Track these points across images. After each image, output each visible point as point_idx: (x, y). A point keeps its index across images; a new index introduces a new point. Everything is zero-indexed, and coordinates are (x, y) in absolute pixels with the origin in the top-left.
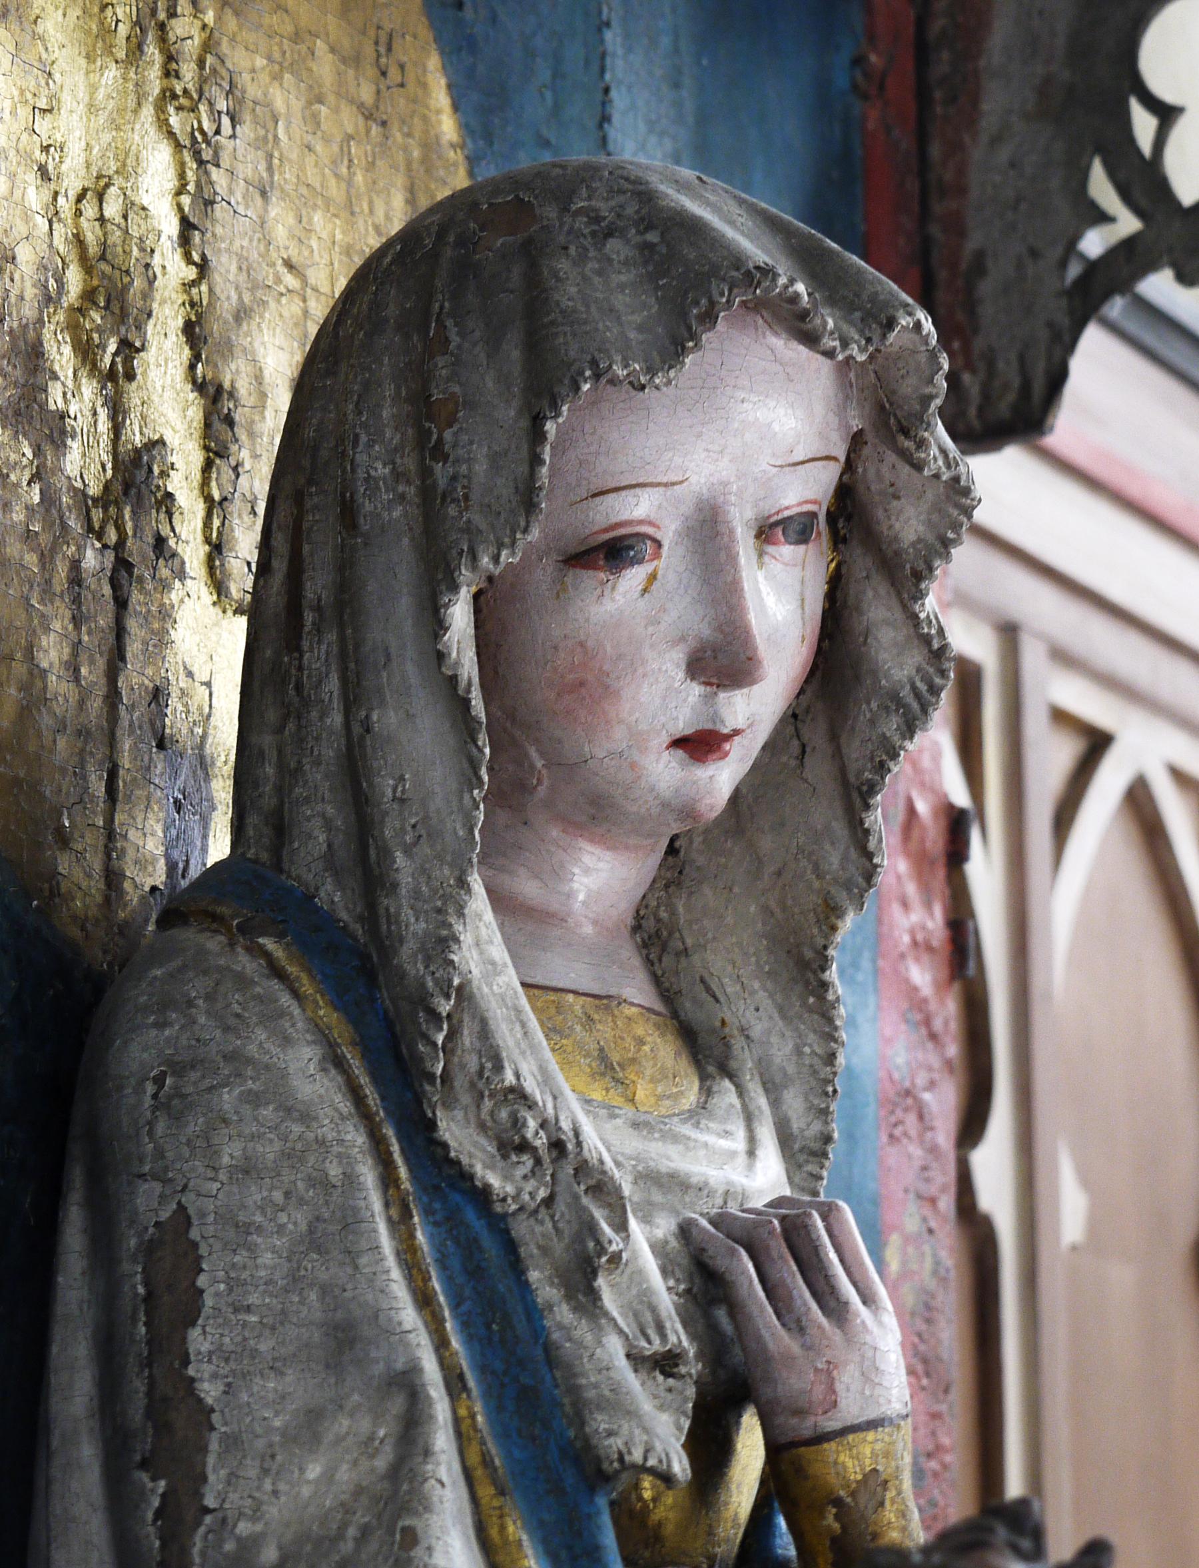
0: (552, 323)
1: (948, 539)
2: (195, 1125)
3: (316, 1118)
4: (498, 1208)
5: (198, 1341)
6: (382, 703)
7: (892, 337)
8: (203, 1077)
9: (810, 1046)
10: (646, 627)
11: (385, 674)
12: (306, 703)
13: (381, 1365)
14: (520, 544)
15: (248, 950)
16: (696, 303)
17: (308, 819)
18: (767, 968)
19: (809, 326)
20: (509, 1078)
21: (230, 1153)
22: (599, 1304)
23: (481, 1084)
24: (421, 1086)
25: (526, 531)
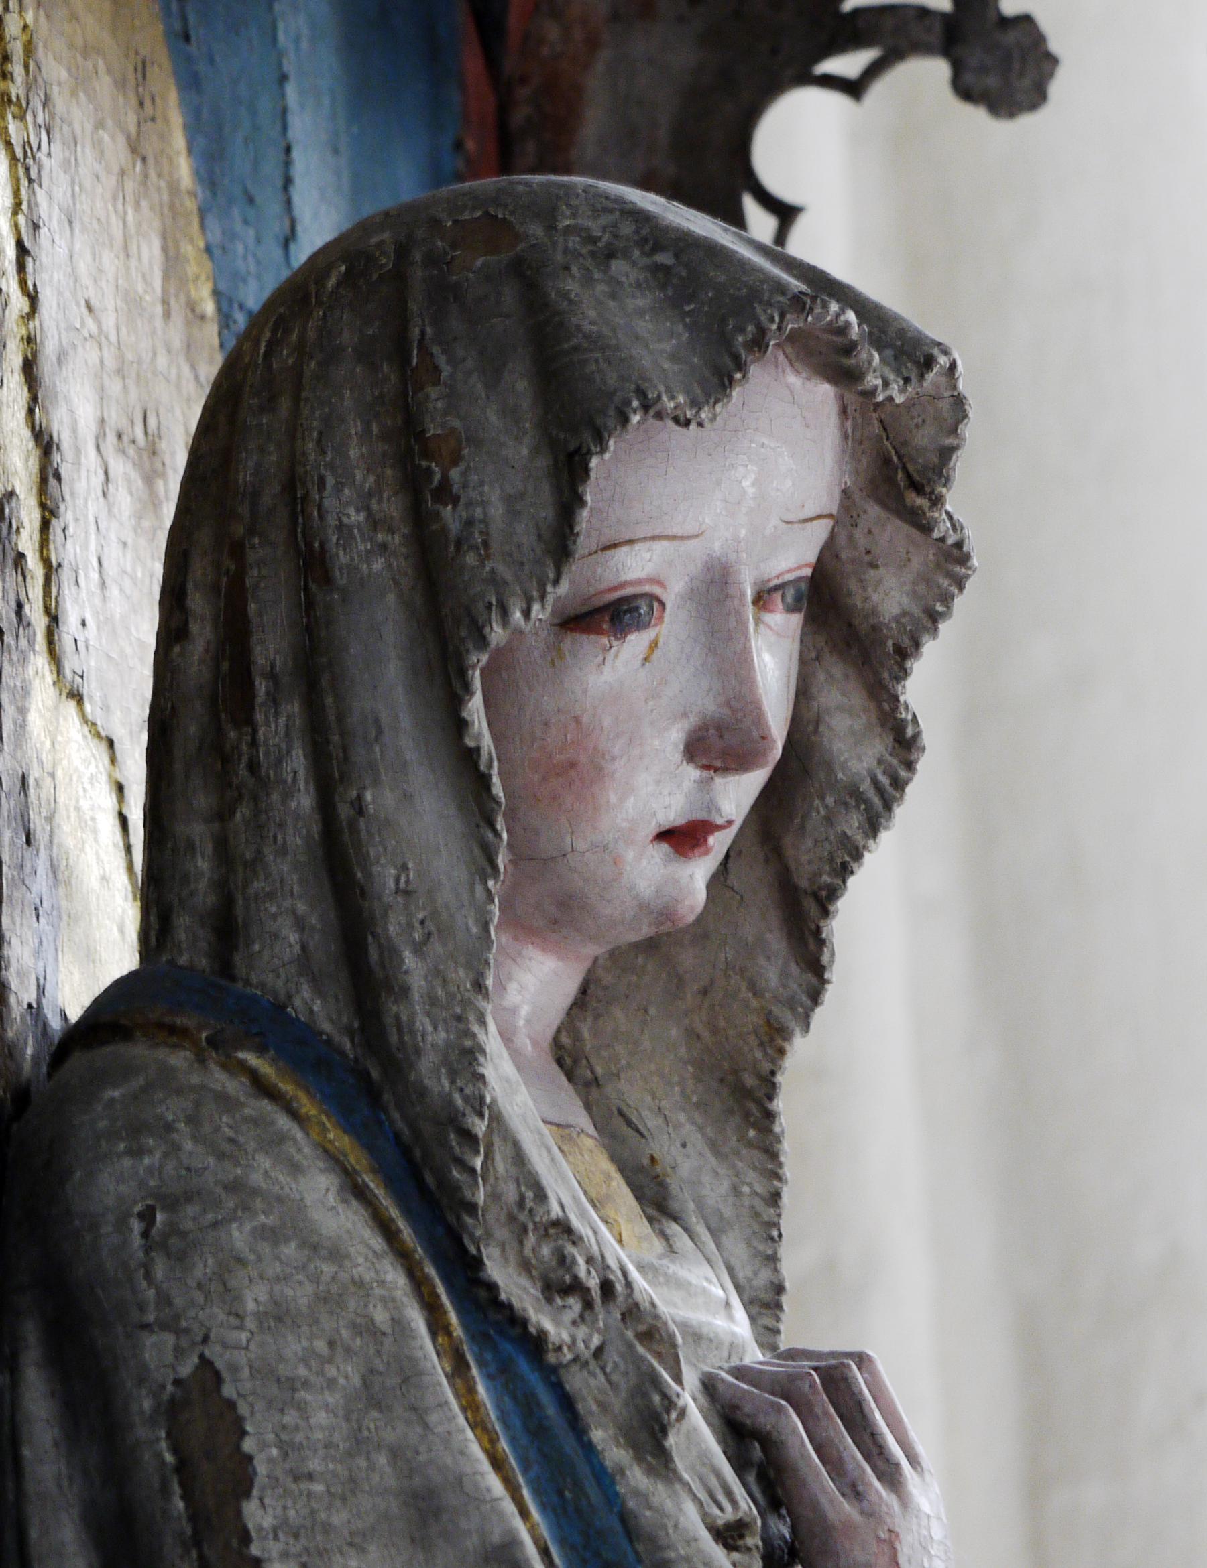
0: (576, 349)
1: (937, 612)
2: (204, 1266)
3: (347, 1256)
4: (551, 1358)
5: (257, 1514)
6: (376, 782)
7: (930, 376)
8: (204, 1211)
9: (750, 1185)
10: (646, 701)
11: (377, 749)
12: (264, 784)
13: (475, 1539)
14: (550, 599)
15: (224, 1067)
16: (742, 330)
17: (274, 917)
18: (695, 1099)
19: (853, 361)
20: (556, 1211)
21: (254, 1298)
22: (671, 1466)
23: (523, 1217)
24: (458, 1218)
25: (556, 582)
